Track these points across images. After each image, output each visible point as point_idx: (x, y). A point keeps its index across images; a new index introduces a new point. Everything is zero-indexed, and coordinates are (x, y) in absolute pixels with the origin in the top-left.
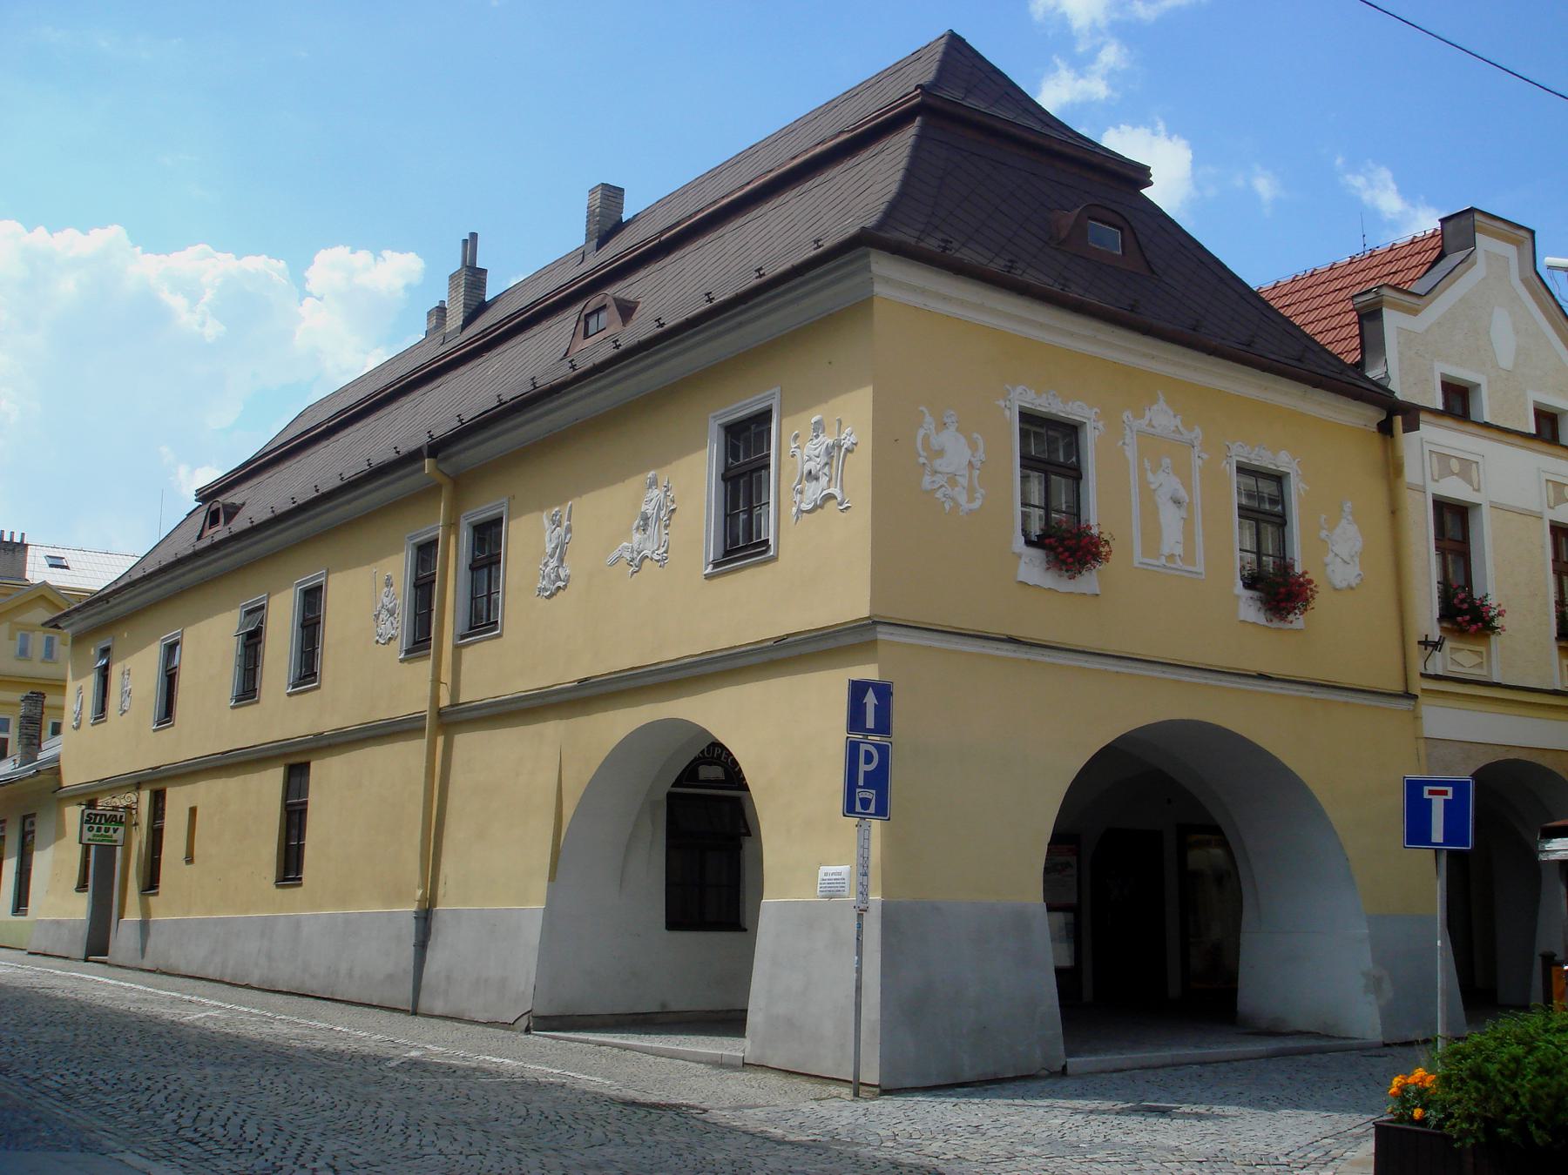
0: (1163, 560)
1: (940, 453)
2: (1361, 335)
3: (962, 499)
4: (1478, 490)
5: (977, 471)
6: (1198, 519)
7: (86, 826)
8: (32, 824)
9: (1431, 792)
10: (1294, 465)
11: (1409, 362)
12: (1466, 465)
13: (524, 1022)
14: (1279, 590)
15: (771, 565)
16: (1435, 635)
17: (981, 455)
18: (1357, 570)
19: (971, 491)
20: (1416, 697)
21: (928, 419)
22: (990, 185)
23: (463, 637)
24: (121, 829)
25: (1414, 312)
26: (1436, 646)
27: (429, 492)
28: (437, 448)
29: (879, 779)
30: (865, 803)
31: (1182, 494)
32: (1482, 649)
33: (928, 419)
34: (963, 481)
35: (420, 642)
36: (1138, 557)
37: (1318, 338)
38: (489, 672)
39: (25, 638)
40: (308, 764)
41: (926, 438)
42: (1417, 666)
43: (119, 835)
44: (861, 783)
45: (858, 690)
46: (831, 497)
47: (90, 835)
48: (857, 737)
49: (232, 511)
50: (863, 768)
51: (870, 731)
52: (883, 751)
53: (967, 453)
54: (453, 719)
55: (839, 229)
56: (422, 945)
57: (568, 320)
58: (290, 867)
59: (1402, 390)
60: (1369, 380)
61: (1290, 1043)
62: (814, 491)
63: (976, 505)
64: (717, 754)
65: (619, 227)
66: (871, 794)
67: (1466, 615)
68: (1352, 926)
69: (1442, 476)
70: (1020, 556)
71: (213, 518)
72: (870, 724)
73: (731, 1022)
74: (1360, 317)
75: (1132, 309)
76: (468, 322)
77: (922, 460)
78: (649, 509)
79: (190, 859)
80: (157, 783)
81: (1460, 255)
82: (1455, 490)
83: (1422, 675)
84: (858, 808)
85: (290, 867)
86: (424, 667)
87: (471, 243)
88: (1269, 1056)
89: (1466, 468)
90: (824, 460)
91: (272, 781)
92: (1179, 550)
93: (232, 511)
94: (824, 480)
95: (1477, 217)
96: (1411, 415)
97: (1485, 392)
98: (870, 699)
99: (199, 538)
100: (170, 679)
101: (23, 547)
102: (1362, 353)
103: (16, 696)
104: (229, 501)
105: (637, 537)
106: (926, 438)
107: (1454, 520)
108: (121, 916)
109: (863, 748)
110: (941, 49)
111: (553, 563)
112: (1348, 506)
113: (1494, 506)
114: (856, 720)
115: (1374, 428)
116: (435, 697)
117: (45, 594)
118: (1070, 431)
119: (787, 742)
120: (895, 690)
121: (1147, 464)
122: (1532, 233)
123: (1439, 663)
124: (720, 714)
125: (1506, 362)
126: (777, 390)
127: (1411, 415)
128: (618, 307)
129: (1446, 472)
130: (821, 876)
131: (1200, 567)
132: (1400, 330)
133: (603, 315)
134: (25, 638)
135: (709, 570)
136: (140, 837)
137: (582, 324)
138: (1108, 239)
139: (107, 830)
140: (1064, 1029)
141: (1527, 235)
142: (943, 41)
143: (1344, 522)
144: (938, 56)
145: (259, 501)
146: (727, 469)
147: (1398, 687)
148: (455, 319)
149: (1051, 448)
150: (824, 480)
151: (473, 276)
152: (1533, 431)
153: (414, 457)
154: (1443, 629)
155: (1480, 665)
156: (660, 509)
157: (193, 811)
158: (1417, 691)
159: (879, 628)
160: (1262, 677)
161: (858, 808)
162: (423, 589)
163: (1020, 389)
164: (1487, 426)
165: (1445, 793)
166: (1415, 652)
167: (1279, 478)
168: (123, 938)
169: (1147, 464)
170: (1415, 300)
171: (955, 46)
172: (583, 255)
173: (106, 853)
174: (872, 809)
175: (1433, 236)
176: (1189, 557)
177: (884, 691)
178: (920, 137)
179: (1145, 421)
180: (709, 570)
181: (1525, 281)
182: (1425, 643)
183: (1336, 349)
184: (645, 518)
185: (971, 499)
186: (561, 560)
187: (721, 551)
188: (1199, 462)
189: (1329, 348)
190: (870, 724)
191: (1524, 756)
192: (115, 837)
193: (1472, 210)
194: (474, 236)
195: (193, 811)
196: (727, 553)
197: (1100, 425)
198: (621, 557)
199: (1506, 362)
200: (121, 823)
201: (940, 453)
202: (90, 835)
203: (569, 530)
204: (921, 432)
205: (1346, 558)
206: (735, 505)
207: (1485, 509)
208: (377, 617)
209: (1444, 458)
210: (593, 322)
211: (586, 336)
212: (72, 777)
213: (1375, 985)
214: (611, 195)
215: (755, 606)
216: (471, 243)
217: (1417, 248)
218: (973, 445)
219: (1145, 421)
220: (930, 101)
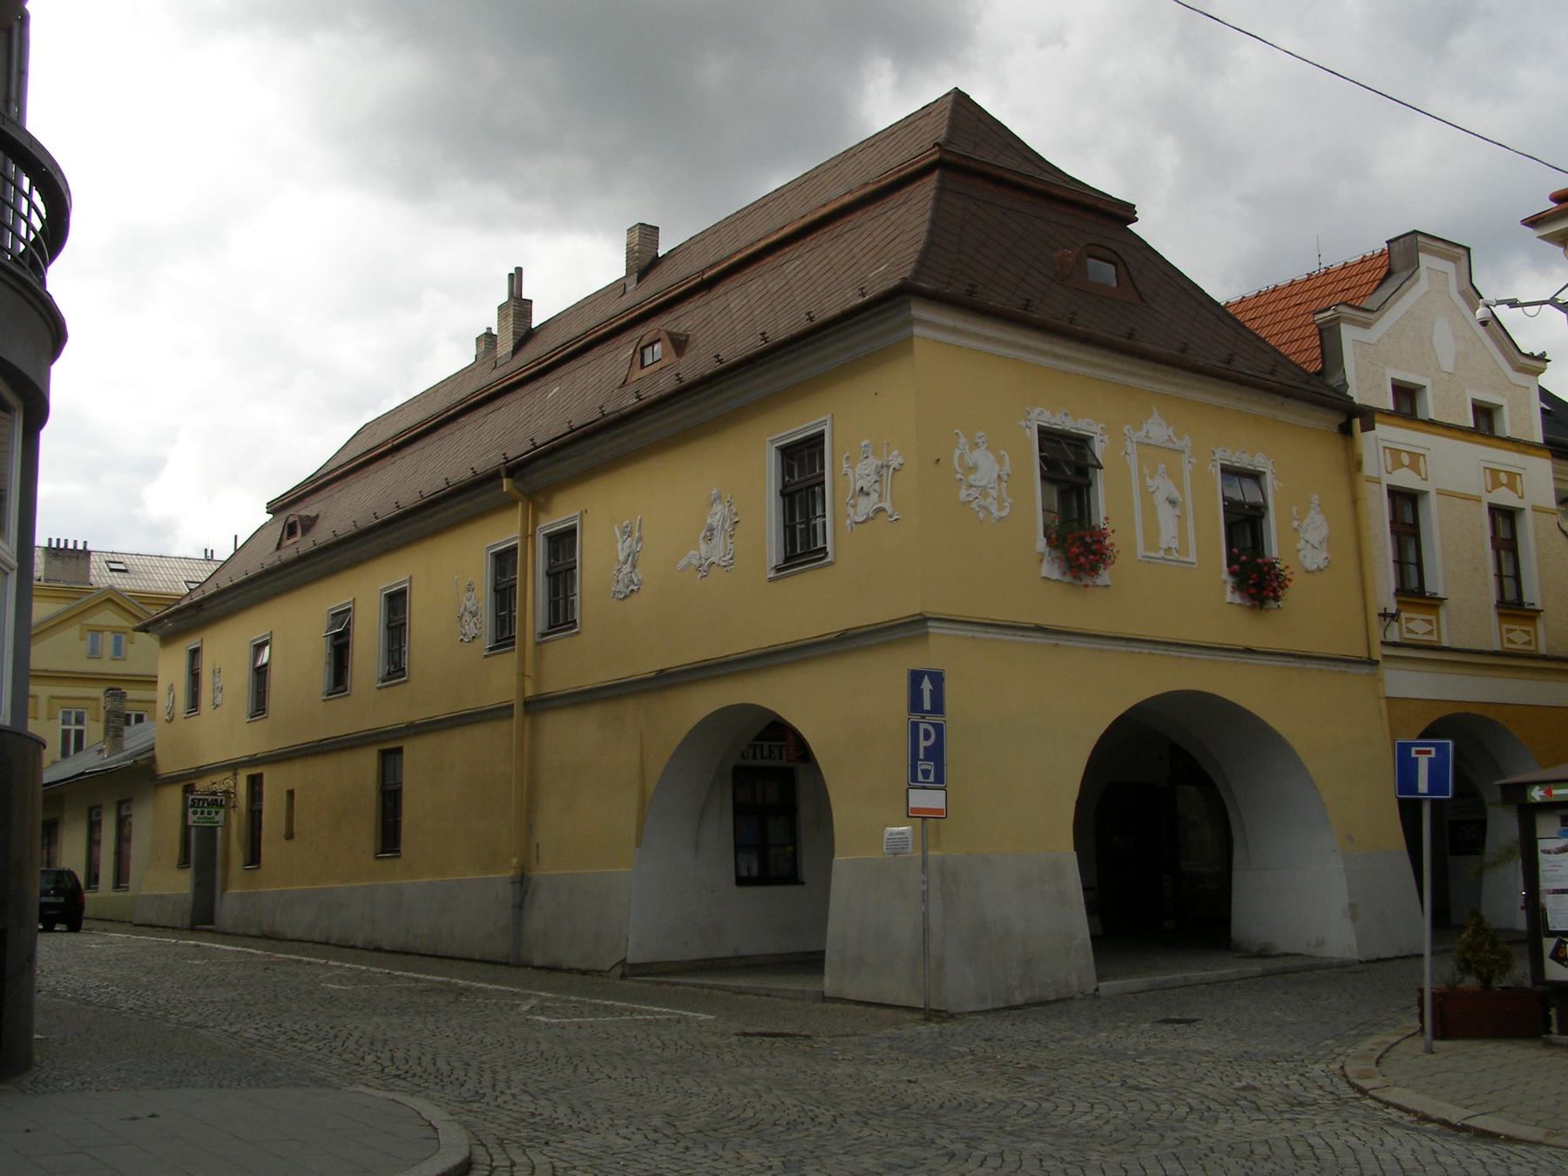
0: (1162, 554)
1: (973, 469)
2: (1322, 345)
3: (994, 509)
5: (1001, 483)
6: (1190, 516)
8: (99, 814)
12: (1415, 457)
13: (618, 971)
14: (1257, 578)
15: (829, 569)
16: (1392, 609)
17: (1007, 468)
19: (1000, 501)
21: (963, 440)
22: (999, 230)
23: (544, 635)
24: (222, 811)
25: (1367, 325)
26: (1395, 617)
27: (508, 504)
29: (936, 753)
30: (926, 773)
31: (1176, 495)
33: (963, 440)
34: (994, 493)
35: (504, 636)
36: (1141, 551)
37: (1282, 349)
38: (572, 663)
39: (94, 642)
40: (399, 750)
42: (1377, 636)
43: (220, 818)
45: (916, 677)
46: (880, 510)
48: (916, 718)
49: (309, 523)
50: (923, 744)
52: (939, 729)
53: (997, 467)
54: (537, 705)
55: (882, 276)
56: (520, 906)
57: (623, 350)
58: (389, 838)
59: (1359, 393)
60: (1329, 387)
61: (1281, 963)
62: (865, 506)
63: (1004, 513)
64: (778, 732)
66: (930, 766)
67: (1413, 592)
68: (1325, 869)
71: (291, 530)
72: (927, 706)
73: (812, 962)
74: (1320, 332)
75: (1130, 336)
76: (518, 347)
78: (714, 521)
79: (290, 836)
80: (255, 767)
81: (1405, 274)
82: (1405, 479)
83: (1383, 643)
84: (920, 778)
85: (389, 838)
87: (516, 278)
88: (1265, 975)
89: (1415, 461)
90: (874, 478)
91: (368, 760)
93: (309, 523)
94: (874, 496)
95: (1420, 238)
96: (1368, 417)
97: (1429, 392)
98: (926, 685)
99: (279, 547)
100: (195, 677)
102: (1323, 362)
103: (98, 692)
104: (304, 513)
105: (703, 547)
107: (1405, 502)
108: (224, 889)
109: (922, 727)
110: (949, 106)
111: (627, 568)
112: (1315, 499)
113: (1440, 493)
114: (915, 704)
115: (1336, 430)
116: (522, 689)
117: (112, 599)
118: (1081, 443)
119: (850, 718)
120: (946, 676)
121: (1146, 471)
122: (1468, 250)
124: (791, 698)
125: (1448, 366)
127: (1368, 417)
128: (672, 340)
129: (1398, 464)
130: (886, 836)
131: (1192, 558)
133: (657, 347)
134: (94, 642)
136: (237, 820)
137: (638, 356)
138: (1103, 273)
140: (1096, 958)
141: (1463, 252)
142: (950, 98)
143: (1312, 513)
144: (947, 113)
146: (785, 486)
147: (1362, 654)
148: (505, 346)
149: (1067, 465)
150: (874, 496)
151: (518, 306)
152: (1472, 425)
154: (1399, 602)
156: (724, 521)
157: (291, 793)
158: (1377, 656)
160: (1248, 651)
161: (920, 778)
162: (504, 595)
163: (1037, 410)
166: (1375, 621)
167: (1256, 477)
168: (228, 907)
169: (1146, 471)
170: (1366, 314)
171: (959, 99)
172: (618, 288)
173: (208, 835)
174: (932, 778)
175: (1381, 255)
176: (1183, 550)
177: (937, 678)
178: (941, 189)
179: (1143, 433)
181: (1462, 293)
182: (1384, 615)
183: (1298, 359)
184: (711, 529)
185: (1001, 508)
186: (634, 566)
187: (782, 557)
188: (1189, 467)
189: (1293, 358)
190: (927, 706)
191: (1472, 710)
192: (217, 818)
193: (1415, 232)
194: (519, 270)
195: (291, 793)
196: (787, 559)
198: (690, 563)
199: (1448, 366)
201: (973, 469)
204: (957, 453)
206: (792, 518)
207: (1433, 494)
208: (461, 618)
209: (1395, 453)
210: (648, 351)
211: (642, 366)
212: (166, 766)
213: (1353, 912)
215: (811, 604)
216: (516, 278)
217: (1368, 265)
219: (1143, 433)
220: (947, 157)
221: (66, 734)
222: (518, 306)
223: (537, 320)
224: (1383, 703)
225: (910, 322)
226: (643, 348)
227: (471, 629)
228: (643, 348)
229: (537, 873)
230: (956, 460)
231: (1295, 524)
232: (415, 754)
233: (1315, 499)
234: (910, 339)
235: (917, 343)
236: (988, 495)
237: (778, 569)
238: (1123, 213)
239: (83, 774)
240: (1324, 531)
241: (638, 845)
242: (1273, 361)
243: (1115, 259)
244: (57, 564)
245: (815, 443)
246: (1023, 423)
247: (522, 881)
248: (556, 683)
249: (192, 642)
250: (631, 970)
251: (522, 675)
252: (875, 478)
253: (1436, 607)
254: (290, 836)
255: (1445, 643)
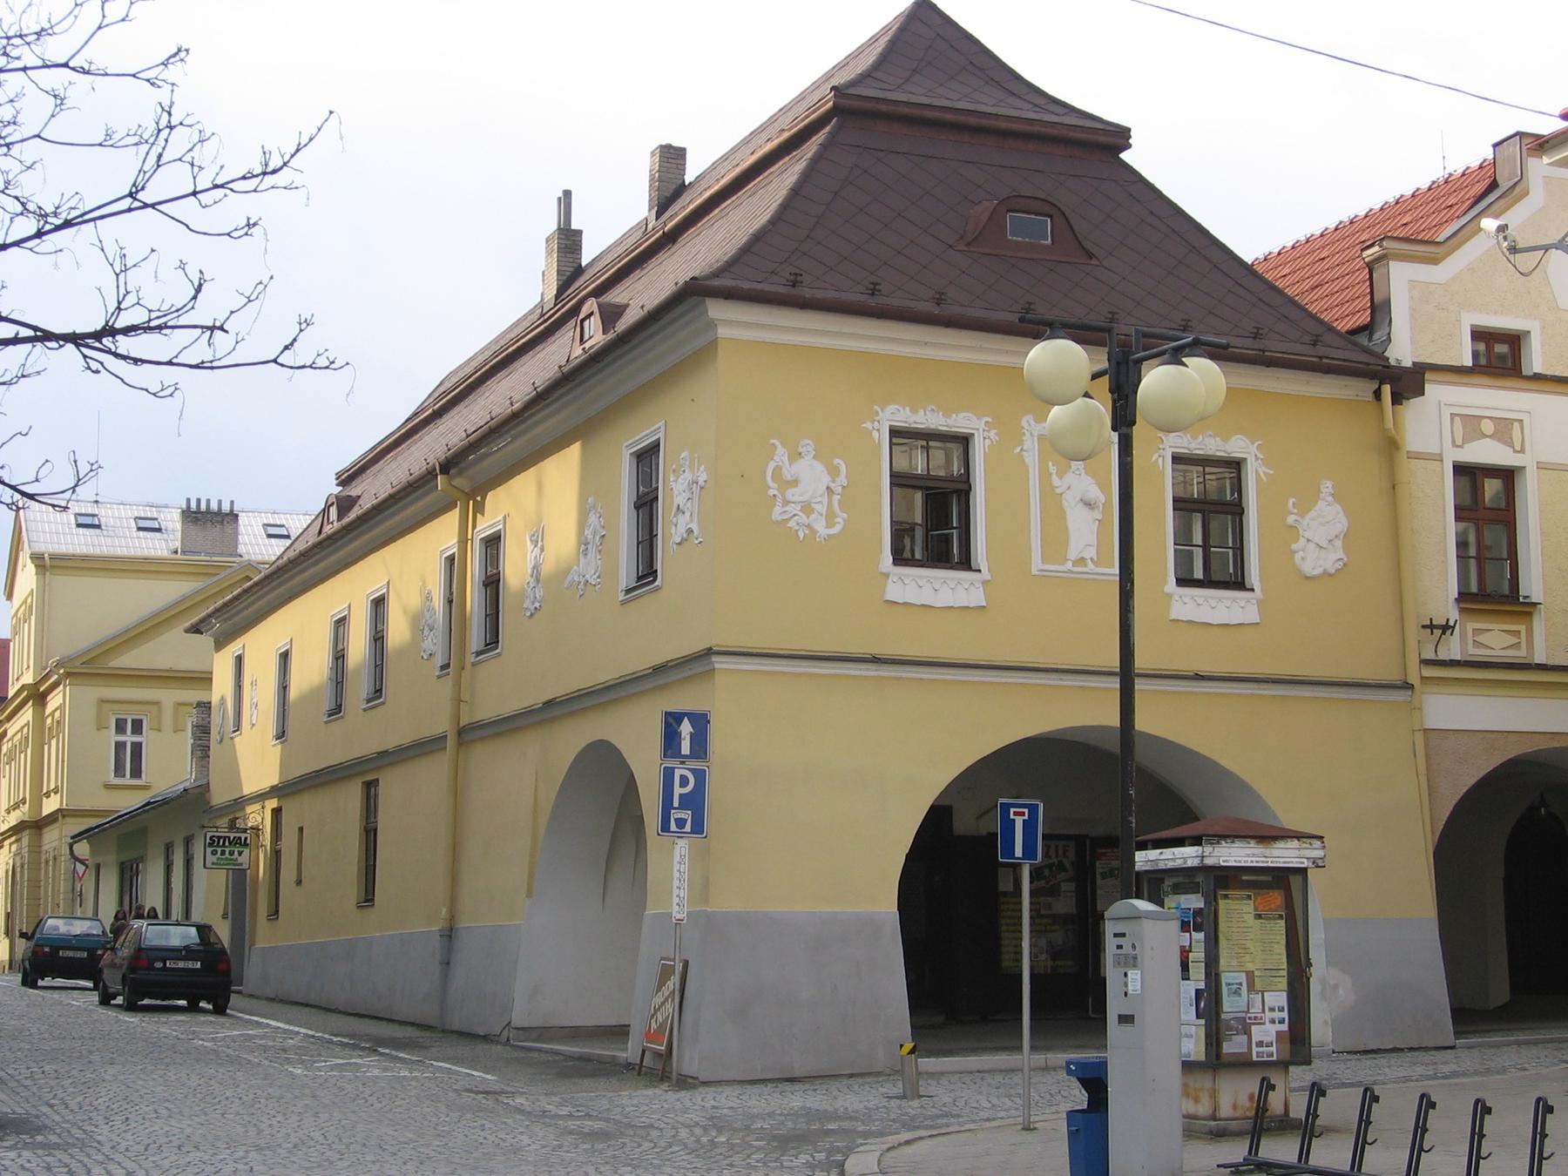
4: (1522, 451)
7: (209, 850)
9: (1016, 814)
10: (1253, 449)
11: (1425, 315)
18: (1340, 554)
19: (830, 519)
20: (1412, 687)
21: (780, 450)
24: (246, 851)
25: (1434, 261)
28: (447, 466)
29: (695, 802)
30: (681, 823)
32: (1522, 628)
33: (780, 450)
36: (1036, 564)
41: (778, 469)
43: (244, 859)
44: (676, 804)
45: (672, 722)
47: (214, 859)
50: (678, 791)
51: (686, 757)
52: (700, 776)
54: (468, 734)
63: (837, 529)
65: (682, 189)
66: (686, 815)
69: (1466, 440)
70: (887, 575)
72: (686, 748)
77: (771, 492)
79: (299, 882)
84: (673, 827)
86: (448, 682)
89: (1504, 429)
91: (350, 797)
92: (1091, 553)
101: (233, 516)
106: (778, 469)
109: (678, 773)
113: (1541, 466)
116: (457, 717)
123: (1453, 648)
126: (661, 423)
132: (1413, 284)
135: (622, 597)
139: (232, 853)
143: (1321, 504)
145: (372, 490)
147: (1394, 676)
151: (568, 240)
153: (430, 475)
155: (1517, 646)
157: (301, 829)
158: (1414, 678)
159: (715, 658)
160: (1198, 677)
164: (1537, 377)
165: (1023, 814)
169: (1052, 469)
174: (688, 828)
177: (701, 722)
180: (622, 597)
185: (830, 524)
190: (686, 748)
192: (240, 860)
194: (568, 194)
195: (301, 829)
197: (992, 433)
200: (246, 845)
201: (795, 482)
202: (214, 859)
203: (542, 550)
204: (772, 465)
205: (1324, 543)
210: (586, 323)
214: (671, 157)
218: (833, 471)
221: (120, 746)
222: (568, 240)
223: (589, 252)
224: (1419, 737)
225: (712, 325)
226: (582, 321)
227: (428, 645)
228: (582, 321)
229: (463, 923)
230: (769, 473)
231: (1291, 519)
232: (392, 786)
233: (1327, 487)
234: (714, 342)
235: (722, 349)
236: (812, 511)
237: (628, 591)
238: (1119, 137)
239: (148, 803)
240: (1341, 524)
241: (529, 895)
242: (1309, 329)
243: (1047, 209)
244: (194, 530)
245: (654, 449)
246: (868, 425)
247: (449, 934)
248: (489, 706)
249: (234, 648)
250: (452, 1032)
251: (458, 701)
252: (688, 495)
253: (1530, 614)
254: (299, 882)
255: (1539, 658)
